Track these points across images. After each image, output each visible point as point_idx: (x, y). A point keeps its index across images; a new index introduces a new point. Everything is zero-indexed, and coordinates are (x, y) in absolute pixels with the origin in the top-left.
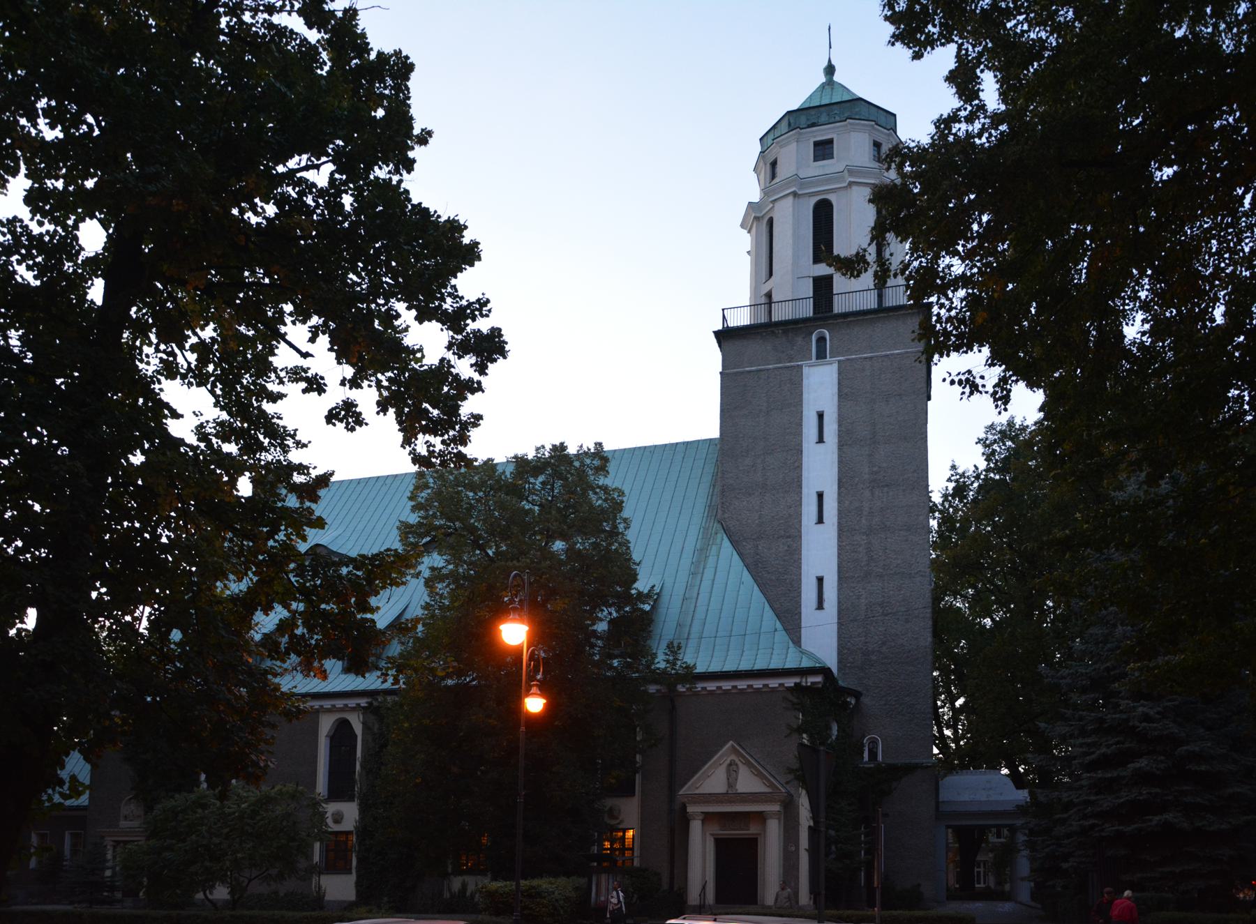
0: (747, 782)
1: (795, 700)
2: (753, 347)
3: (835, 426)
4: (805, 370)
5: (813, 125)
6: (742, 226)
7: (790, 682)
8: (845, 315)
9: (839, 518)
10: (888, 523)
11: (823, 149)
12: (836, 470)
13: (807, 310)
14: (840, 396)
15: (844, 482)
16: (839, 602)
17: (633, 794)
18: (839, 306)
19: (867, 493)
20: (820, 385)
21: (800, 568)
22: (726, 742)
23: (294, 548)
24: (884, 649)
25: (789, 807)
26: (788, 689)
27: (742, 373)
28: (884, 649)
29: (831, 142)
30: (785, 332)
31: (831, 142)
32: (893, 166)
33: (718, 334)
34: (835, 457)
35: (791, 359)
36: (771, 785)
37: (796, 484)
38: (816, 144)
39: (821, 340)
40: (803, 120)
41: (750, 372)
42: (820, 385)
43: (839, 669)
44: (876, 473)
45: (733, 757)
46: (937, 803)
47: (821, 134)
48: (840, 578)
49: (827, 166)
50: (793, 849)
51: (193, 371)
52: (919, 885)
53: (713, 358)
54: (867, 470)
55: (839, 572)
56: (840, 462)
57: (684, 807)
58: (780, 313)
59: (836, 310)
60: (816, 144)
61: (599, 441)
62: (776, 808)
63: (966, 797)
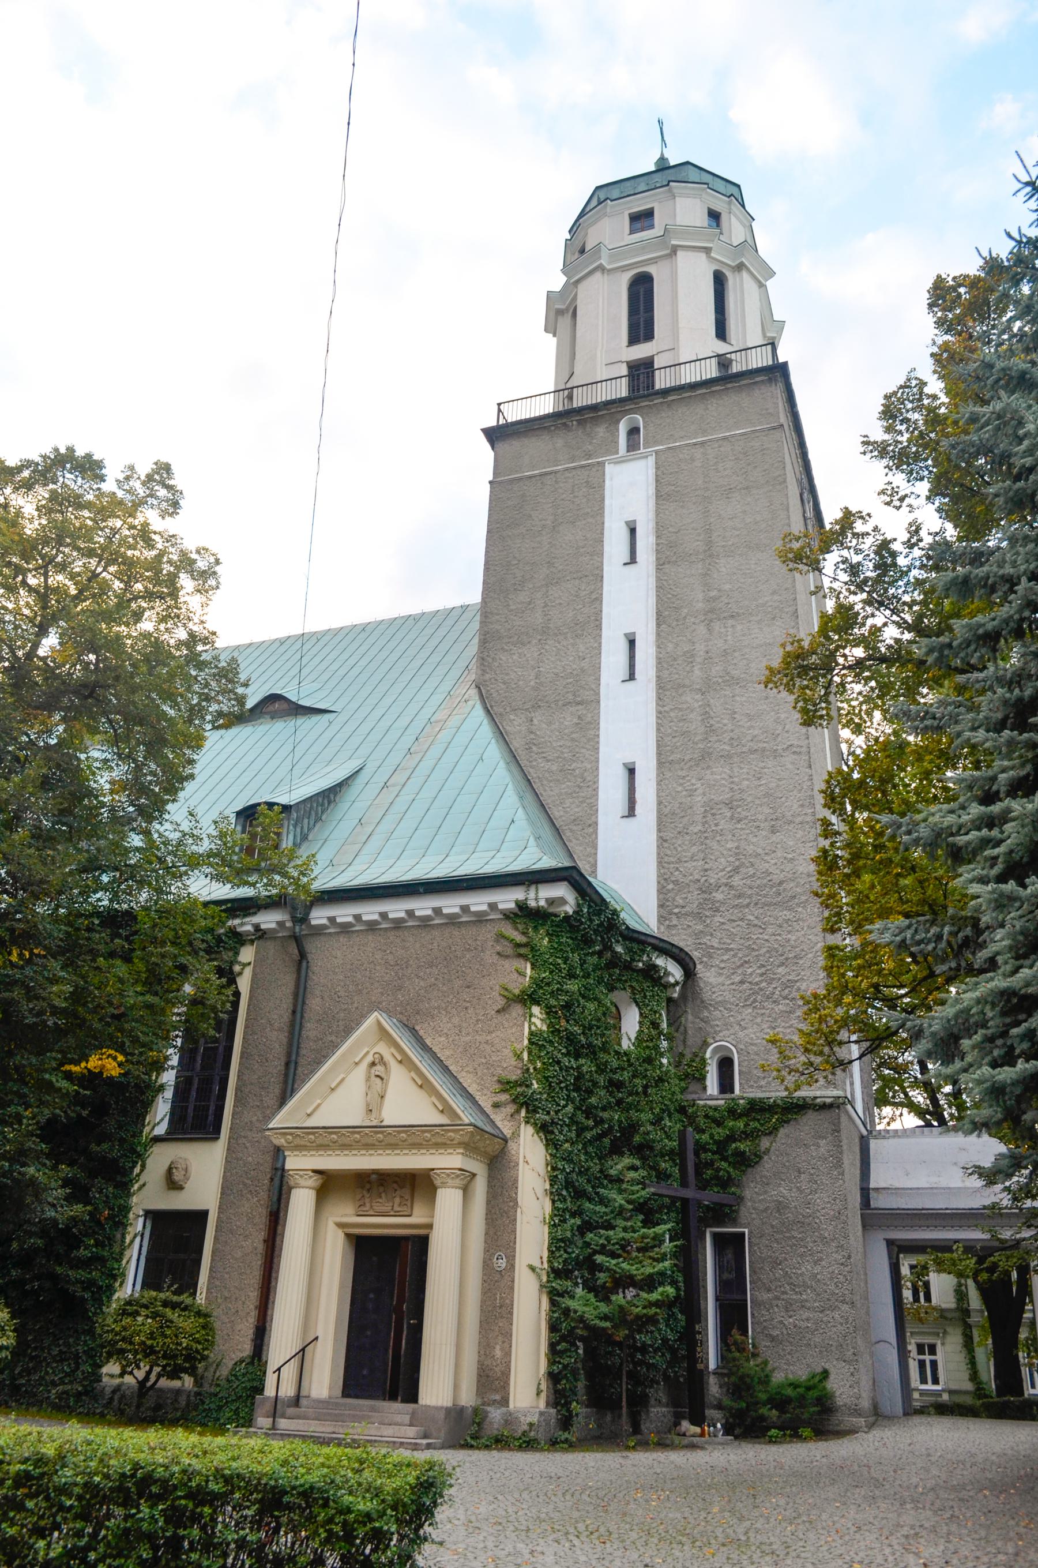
0: (406, 1104)
1: (520, 939)
3: (652, 539)
4: (608, 468)
6: (546, 330)
7: (507, 899)
8: (666, 392)
10: (735, 673)
11: (642, 219)
12: (652, 600)
14: (659, 496)
15: (667, 613)
17: (217, 1130)
18: (662, 381)
19: (702, 629)
20: (629, 487)
21: (597, 749)
22: (364, 1016)
24: (736, 881)
25: (498, 1160)
26: (507, 916)
27: (520, 479)
28: (736, 881)
29: (649, 214)
31: (649, 214)
32: (907, 636)
33: (494, 435)
34: (652, 581)
36: (446, 1109)
37: (591, 624)
39: (633, 431)
41: (530, 477)
42: (629, 487)
44: (715, 599)
45: (384, 1050)
46: (865, 1192)
47: (639, 205)
48: (660, 764)
50: (503, 1263)
52: (825, 1374)
53: (473, 470)
54: (700, 596)
55: (659, 754)
56: (659, 588)
57: (278, 1152)
58: (581, 400)
59: (657, 387)
61: (164, 459)
62: (452, 1160)
63: (921, 1180)
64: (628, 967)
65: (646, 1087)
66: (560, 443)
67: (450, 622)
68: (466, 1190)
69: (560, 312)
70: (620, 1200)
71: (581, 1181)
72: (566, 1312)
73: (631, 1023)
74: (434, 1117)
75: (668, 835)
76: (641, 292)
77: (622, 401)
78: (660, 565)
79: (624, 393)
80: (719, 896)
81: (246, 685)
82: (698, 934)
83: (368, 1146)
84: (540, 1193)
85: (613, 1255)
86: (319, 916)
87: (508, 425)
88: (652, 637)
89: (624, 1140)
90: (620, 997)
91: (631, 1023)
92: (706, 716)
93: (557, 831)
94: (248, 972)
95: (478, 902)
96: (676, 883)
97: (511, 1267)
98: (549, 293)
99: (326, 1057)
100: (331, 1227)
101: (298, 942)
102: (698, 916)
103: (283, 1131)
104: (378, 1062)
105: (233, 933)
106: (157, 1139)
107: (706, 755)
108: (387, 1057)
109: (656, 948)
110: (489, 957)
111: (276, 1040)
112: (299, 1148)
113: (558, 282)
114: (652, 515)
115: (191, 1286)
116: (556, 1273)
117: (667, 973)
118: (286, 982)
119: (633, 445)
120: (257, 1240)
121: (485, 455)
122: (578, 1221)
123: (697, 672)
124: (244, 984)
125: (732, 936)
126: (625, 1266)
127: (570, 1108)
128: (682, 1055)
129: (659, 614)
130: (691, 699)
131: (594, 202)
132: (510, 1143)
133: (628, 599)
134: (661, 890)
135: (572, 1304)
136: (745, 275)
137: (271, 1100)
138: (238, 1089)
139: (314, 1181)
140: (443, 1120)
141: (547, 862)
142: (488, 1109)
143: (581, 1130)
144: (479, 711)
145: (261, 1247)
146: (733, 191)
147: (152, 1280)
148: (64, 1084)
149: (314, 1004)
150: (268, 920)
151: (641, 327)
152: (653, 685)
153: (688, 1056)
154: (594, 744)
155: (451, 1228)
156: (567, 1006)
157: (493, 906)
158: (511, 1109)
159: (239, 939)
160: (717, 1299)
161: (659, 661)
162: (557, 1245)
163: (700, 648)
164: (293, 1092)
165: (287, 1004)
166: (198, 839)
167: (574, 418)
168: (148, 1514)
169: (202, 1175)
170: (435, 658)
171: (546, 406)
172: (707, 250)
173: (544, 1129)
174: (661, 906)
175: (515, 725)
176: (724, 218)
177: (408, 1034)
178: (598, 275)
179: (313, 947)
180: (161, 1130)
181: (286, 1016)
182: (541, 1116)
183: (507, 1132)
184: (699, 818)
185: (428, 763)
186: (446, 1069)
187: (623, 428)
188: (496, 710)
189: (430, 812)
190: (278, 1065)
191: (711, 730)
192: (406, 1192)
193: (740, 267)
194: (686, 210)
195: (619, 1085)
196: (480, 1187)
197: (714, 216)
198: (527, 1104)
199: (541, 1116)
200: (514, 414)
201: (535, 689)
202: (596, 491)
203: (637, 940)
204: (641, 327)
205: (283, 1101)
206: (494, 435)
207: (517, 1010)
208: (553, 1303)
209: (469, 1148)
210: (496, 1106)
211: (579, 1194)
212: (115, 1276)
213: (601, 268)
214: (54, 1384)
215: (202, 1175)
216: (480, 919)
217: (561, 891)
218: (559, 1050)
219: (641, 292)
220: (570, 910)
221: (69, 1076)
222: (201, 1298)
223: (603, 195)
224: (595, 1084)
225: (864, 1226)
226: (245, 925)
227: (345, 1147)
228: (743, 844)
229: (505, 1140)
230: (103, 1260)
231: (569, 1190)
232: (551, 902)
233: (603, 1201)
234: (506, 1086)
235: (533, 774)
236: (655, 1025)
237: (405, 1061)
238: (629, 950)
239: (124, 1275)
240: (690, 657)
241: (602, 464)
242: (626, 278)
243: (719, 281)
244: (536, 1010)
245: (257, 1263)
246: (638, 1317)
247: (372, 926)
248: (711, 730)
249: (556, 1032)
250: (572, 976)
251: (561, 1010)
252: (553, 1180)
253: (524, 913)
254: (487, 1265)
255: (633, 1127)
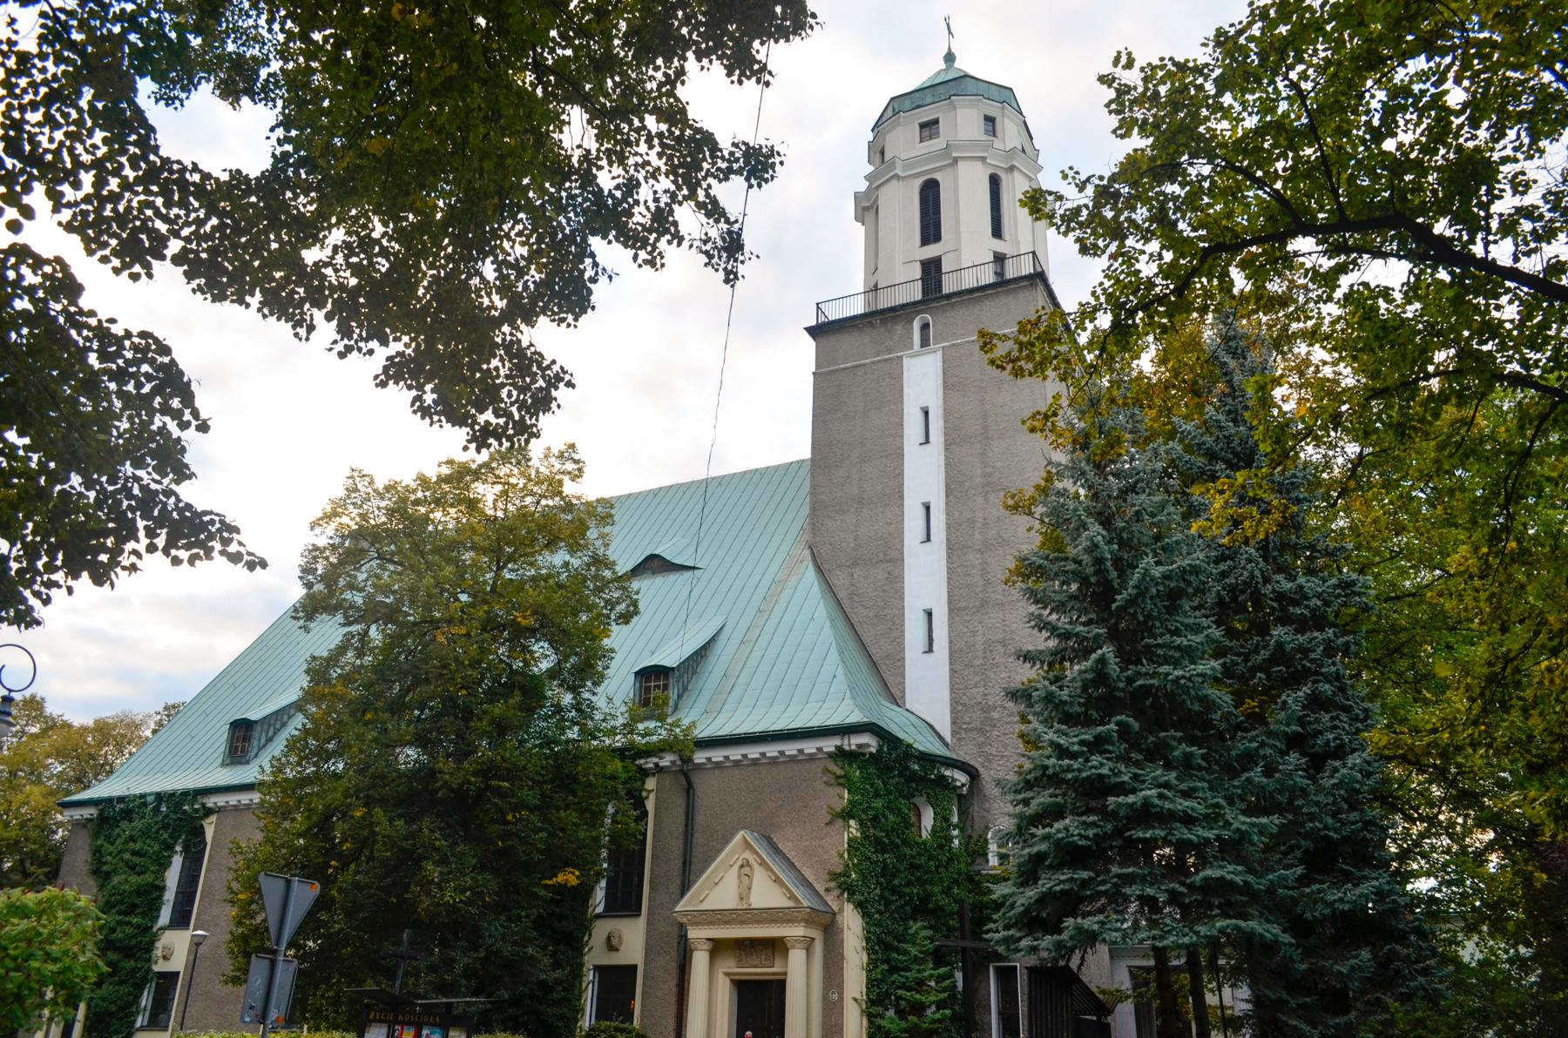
0: (765, 894)
1: (839, 772)
2: (849, 341)
3: (941, 423)
4: (906, 361)
5: (918, 107)
7: (829, 745)
8: (950, 296)
9: (948, 534)
10: (1006, 536)
12: (942, 476)
13: (988, 277)
14: (946, 386)
15: (953, 488)
16: (951, 642)
17: (640, 909)
18: (949, 286)
19: (980, 500)
20: (922, 377)
22: (733, 835)
23: (1119, 653)
25: (829, 927)
26: (830, 755)
29: (936, 122)
30: (884, 321)
31: (936, 122)
33: (813, 331)
35: (890, 351)
36: (792, 897)
37: (896, 495)
38: (923, 126)
39: (925, 327)
40: (907, 104)
42: (922, 377)
43: (954, 733)
44: (990, 474)
45: (748, 855)
47: (926, 115)
48: (951, 611)
49: (936, 144)
51: (1501, 110)
54: (979, 472)
55: (950, 602)
56: (947, 465)
58: (886, 301)
59: (946, 290)
60: (923, 126)
64: (925, 779)
65: (937, 867)
66: (867, 339)
67: (789, 478)
68: (809, 950)
69: (865, 209)
70: (914, 951)
71: (889, 939)
72: (879, 1028)
73: (928, 819)
74: (785, 903)
75: (957, 667)
76: (930, 195)
77: (915, 303)
78: (948, 445)
79: (918, 296)
80: (996, 715)
81: (637, 593)
82: (981, 745)
83: (742, 923)
84: (859, 949)
85: (910, 989)
86: (700, 757)
87: (824, 324)
88: (943, 506)
89: (922, 908)
90: (920, 801)
91: (928, 819)
92: (985, 572)
93: (874, 666)
94: (652, 796)
95: (809, 747)
96: (964, 705)
97: (841, 999)
98: (857, 196)
99: (710, 864)
100: (721, 976)
101: (686, 774)
102: (981, 731)
103: (685, 913)
104: (746, 864)
105: (640, 768)
106: (599, 916)
107: (985, 603)
108: (752, 861)
109: (943, 764)
110: (819, 786)
111: (676, 845)
112: (696, 924)
113: (863, 186)
114: (940, 402)
115: (629, 1017)
116: (872, 1002)
117: (954, 780)
118: (679, 804)
119: (925, 342)
120: (671, 985)
121: (810, 344)
122: (886, 967)
123: (977, 536)
124: (650, 805)
125: (1005, 746)
126: (918, 996)
127: (878, 891)
128: (970, 837)
129: (947, 487)
130: (973, 558)
131: (890, 112)
132: (839, 917)
133: (924, 474)
134: (953, 710)
135: (882, 1022)
136: (1016, 174)
137: (675, 886)
138: (651, 882)
139: (708, 946)
140: (790, 904)
141: (856, 717)
142: (822, 893)
143: (888, 903)
144: (811, 573)
145: (674, 990)
146: (1004, 96)
147: (601, 1014)
148: (543, 893)
149: (700, 819)
150: (667, 760)
151: (931, 230)
152: (944, 546)
153: (975, 837)
154: (900, 594)
155: (800, 975)
156: (875, 819)
157: (820, 750)
158: (837, 892)
159: (644, 773)
160: (999, 1013)
161: (948, 526)
162: (872, 983)
163: (979, 515)
164: (689, 888)
165: (681, 820)
166: (614, 717)
167: (880, 319)
168: (913, 819)
169: (631, 940)
170: (776, 518)
171: (857, 307)
172: (983, 159)
173: (860, 905)
174: (953, 723)
175: (840, 579)
176: (998, 122)
177: (765, 844)
178: (894, 182)
179: (699, 780)
180: (600, 909)
181: (681, 828)
182: (858, 897)
183: (836, 908)
184: (980, 654)
185: (773, 621)
186: (792, 865)
187: (916, 325)
188: (825, 567)
189: (778, 677)
190: (678, 864)
191: (988, 583)
192: (769, 952)
193: (1012, 168)
194: (964, 122)
195: (917, 867)
196: (818, 947)
197: (990, 120)
198: (848, 889)
199: (858, 897)
200: (834, 313)
201: (854, 549)
202: (897, 379)
203: (928, 759)
204: (931, 230)
205: (683, 894)
206: (813, 331)
207: (839, 823)
208: (870, 1022)
209: (809, 922)
210: (827, 890)
211: (887, 947)
212: (579, 1010)
213: (897, 176)
214: (1535, 800)
215: (631, 940)
216: (811, 758)
217: (865, 739)
218: (869, 850)
219: (930, 195)
220: (873, 750)
221: (546, 886)
222: (636, 1023)
223: (898, 106)
224: (898, 870)
225: (1111, 957)
226: (649, 764)
227: (726, 923)
228: (1013, 675)
229: (834, 914)
230: (569, 1000)
231: (880, 946)
232: (860, 746)
233: (906, 953)
234: (834, 876)
235: (855, 619)
236: (946, 820)
237: (763, 864)
238: (923, 768)
239: (583, 1010)
240: (972, 521)
241: (900, 358)
242: (918, 182)
243: (995, 182)
244: (852, 823)
245: (673, 1000)
246: (927, 1030)
247: (737, 763)
248: (988, 583)
249: (866, 837)
250: (877, 795)
251: (871, 822)
252: (868, 940)
253: (841, 754)
254: (825, 998)
255: (926, 899)
